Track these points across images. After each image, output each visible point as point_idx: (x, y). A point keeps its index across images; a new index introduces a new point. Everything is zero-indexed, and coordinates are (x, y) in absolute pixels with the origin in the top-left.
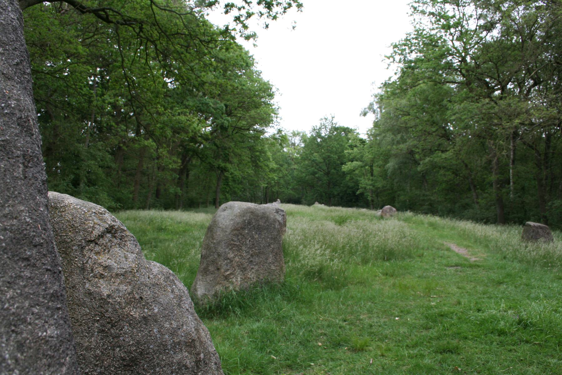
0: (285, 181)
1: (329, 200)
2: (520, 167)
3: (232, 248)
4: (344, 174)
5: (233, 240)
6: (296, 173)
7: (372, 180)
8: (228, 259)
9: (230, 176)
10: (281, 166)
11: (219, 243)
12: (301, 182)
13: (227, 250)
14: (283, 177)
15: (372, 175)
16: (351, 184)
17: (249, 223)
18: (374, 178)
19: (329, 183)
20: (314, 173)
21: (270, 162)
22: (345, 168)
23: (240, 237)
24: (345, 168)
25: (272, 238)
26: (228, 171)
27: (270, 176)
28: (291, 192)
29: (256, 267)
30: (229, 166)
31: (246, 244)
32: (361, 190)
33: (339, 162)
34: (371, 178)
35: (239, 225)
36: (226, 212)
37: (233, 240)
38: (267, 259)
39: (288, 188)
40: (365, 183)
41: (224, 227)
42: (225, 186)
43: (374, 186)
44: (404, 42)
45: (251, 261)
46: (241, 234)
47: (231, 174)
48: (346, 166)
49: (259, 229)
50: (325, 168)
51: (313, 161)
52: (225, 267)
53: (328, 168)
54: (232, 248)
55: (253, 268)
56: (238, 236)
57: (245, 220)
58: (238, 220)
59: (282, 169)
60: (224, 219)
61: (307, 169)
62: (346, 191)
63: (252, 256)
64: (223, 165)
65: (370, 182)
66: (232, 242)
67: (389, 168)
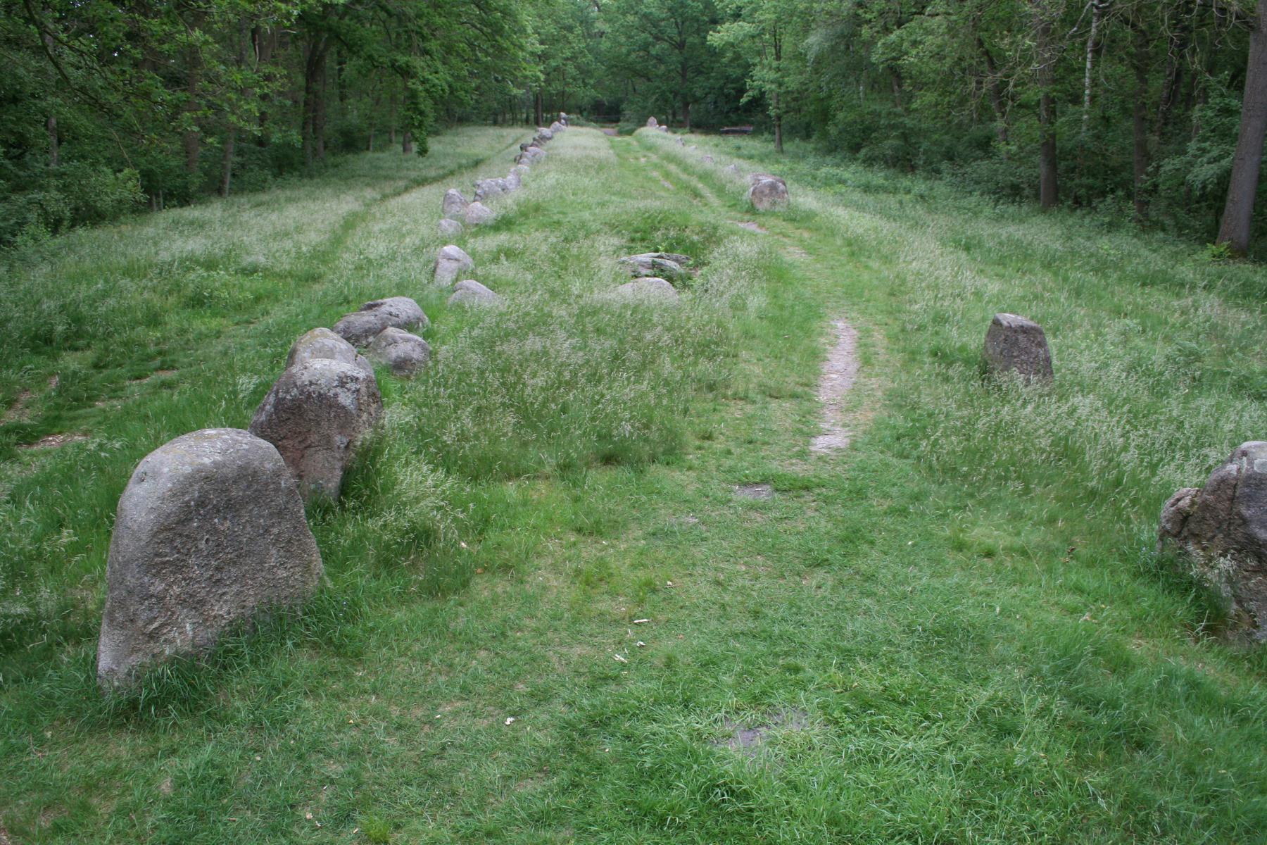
0: (578, 67)
1: (686, 112)
2: (1105, 66)
3: (159, 572)
4: (715, 53)
5: (158, 555)
6: (605, 45)
7: (778, 69)
8: (152, 596)
9: (421, 88)
10: (570, 29)
11: (126, 564)
12: (621, 68)
13: (146, 579)
14: (573, 58)
15: (778, 58)
16: (734, 72)
17: (201, 503)
18: (783, 63)
19: (684, 69)
20: (645, 47)
21: (528, 36)
22: (716, 38)
23: (178, 543)
24: (716, 38)
25: (271, 514)
26: (414, 76)
27: (528, 73)
28: (593, 93)
29: (235, 588)
30: (418, 62)
31: (198, 551)
32: (750, 93)
33: (706, 19)
34: (775, 64)
35: (173, 518)
36: (145, 485)
37: (158, 555)
38: (262, 562)
39: (585, 85)
40: (763, 77)
41: (135, 527)
42: (410, 113)
43: (780, 85)
44: (405, 164)
45: (218, 580)
46: (180, 535)
47: (423, 83)
48: (717, 35)
49: (231, 507)
50: (672, 32)
51: (645, 16)
52: (144, 616)
53: (680, 34)
54: (159, 572)
55: (224, 594)
56: (172, 541)
57: (189, 502)
58: (168, 507)
59: (571, 37)
60: (136, 505)
61: (630, 37)
62: (721, 88)
63: (218, 569)
64: (402, 59)
65: (773, 75)
66: (157, 560)
67: (809, 47)
